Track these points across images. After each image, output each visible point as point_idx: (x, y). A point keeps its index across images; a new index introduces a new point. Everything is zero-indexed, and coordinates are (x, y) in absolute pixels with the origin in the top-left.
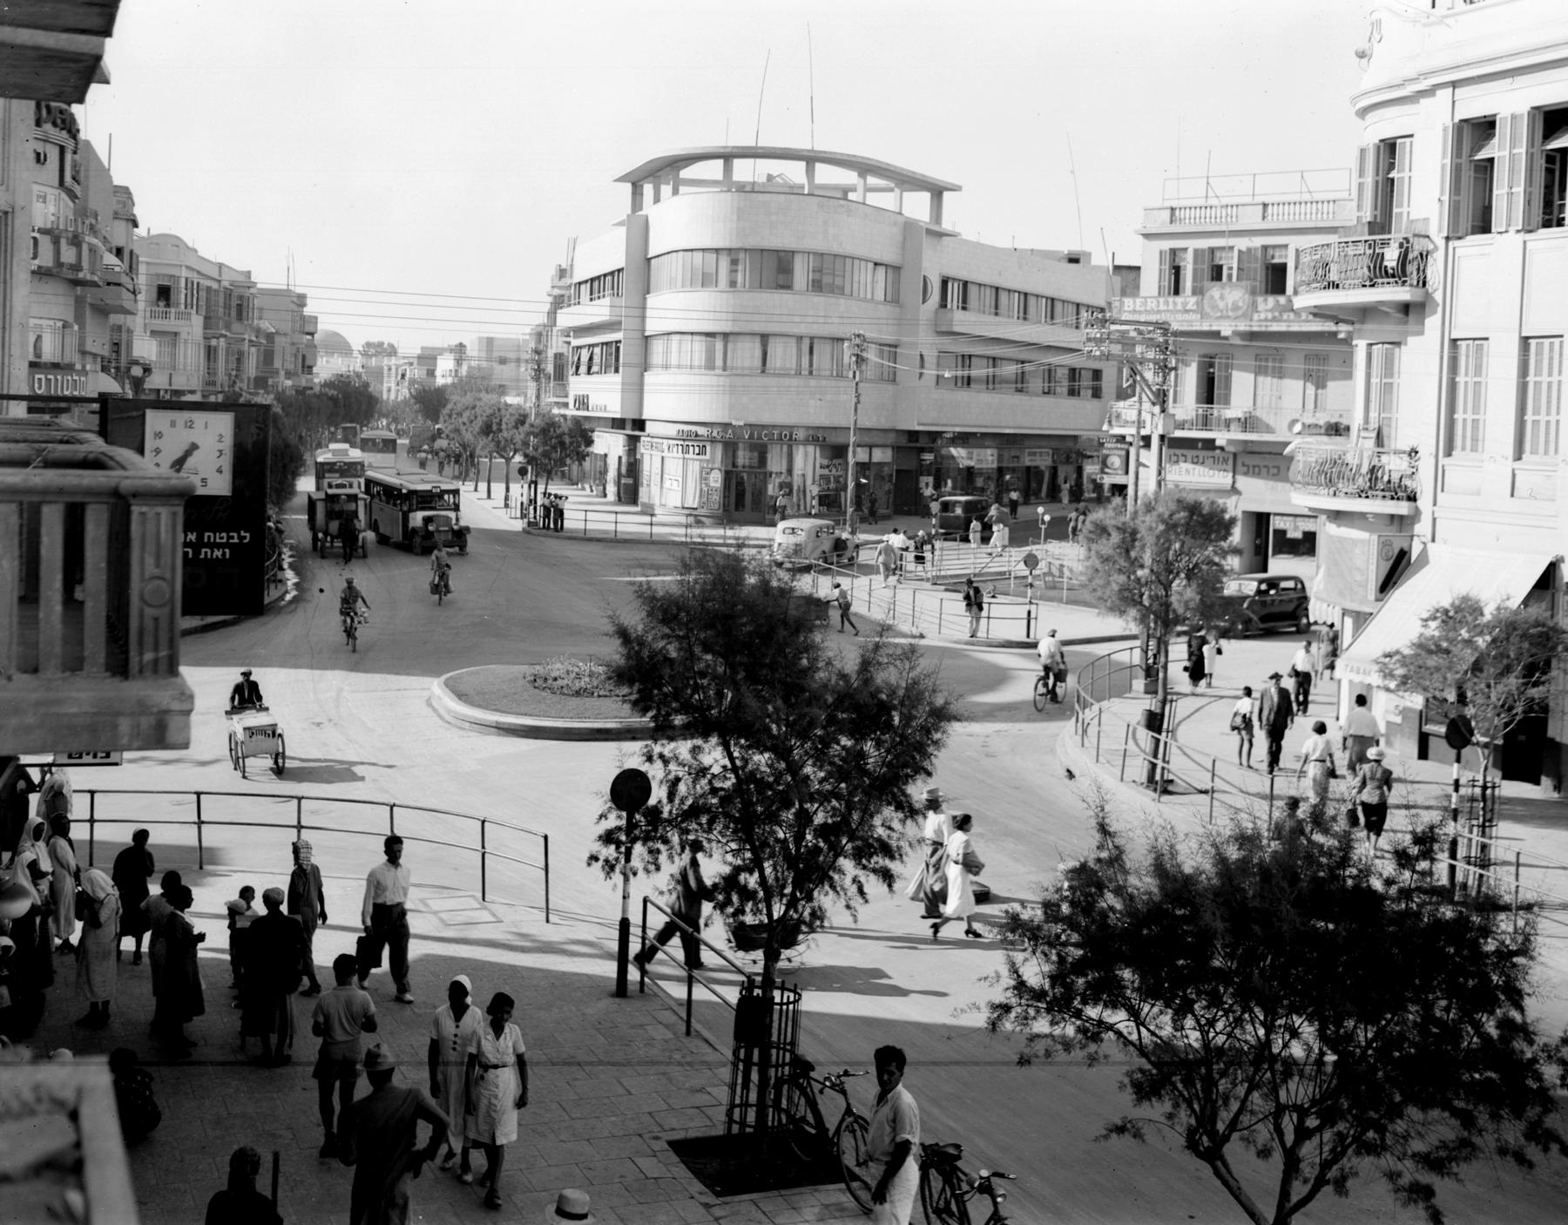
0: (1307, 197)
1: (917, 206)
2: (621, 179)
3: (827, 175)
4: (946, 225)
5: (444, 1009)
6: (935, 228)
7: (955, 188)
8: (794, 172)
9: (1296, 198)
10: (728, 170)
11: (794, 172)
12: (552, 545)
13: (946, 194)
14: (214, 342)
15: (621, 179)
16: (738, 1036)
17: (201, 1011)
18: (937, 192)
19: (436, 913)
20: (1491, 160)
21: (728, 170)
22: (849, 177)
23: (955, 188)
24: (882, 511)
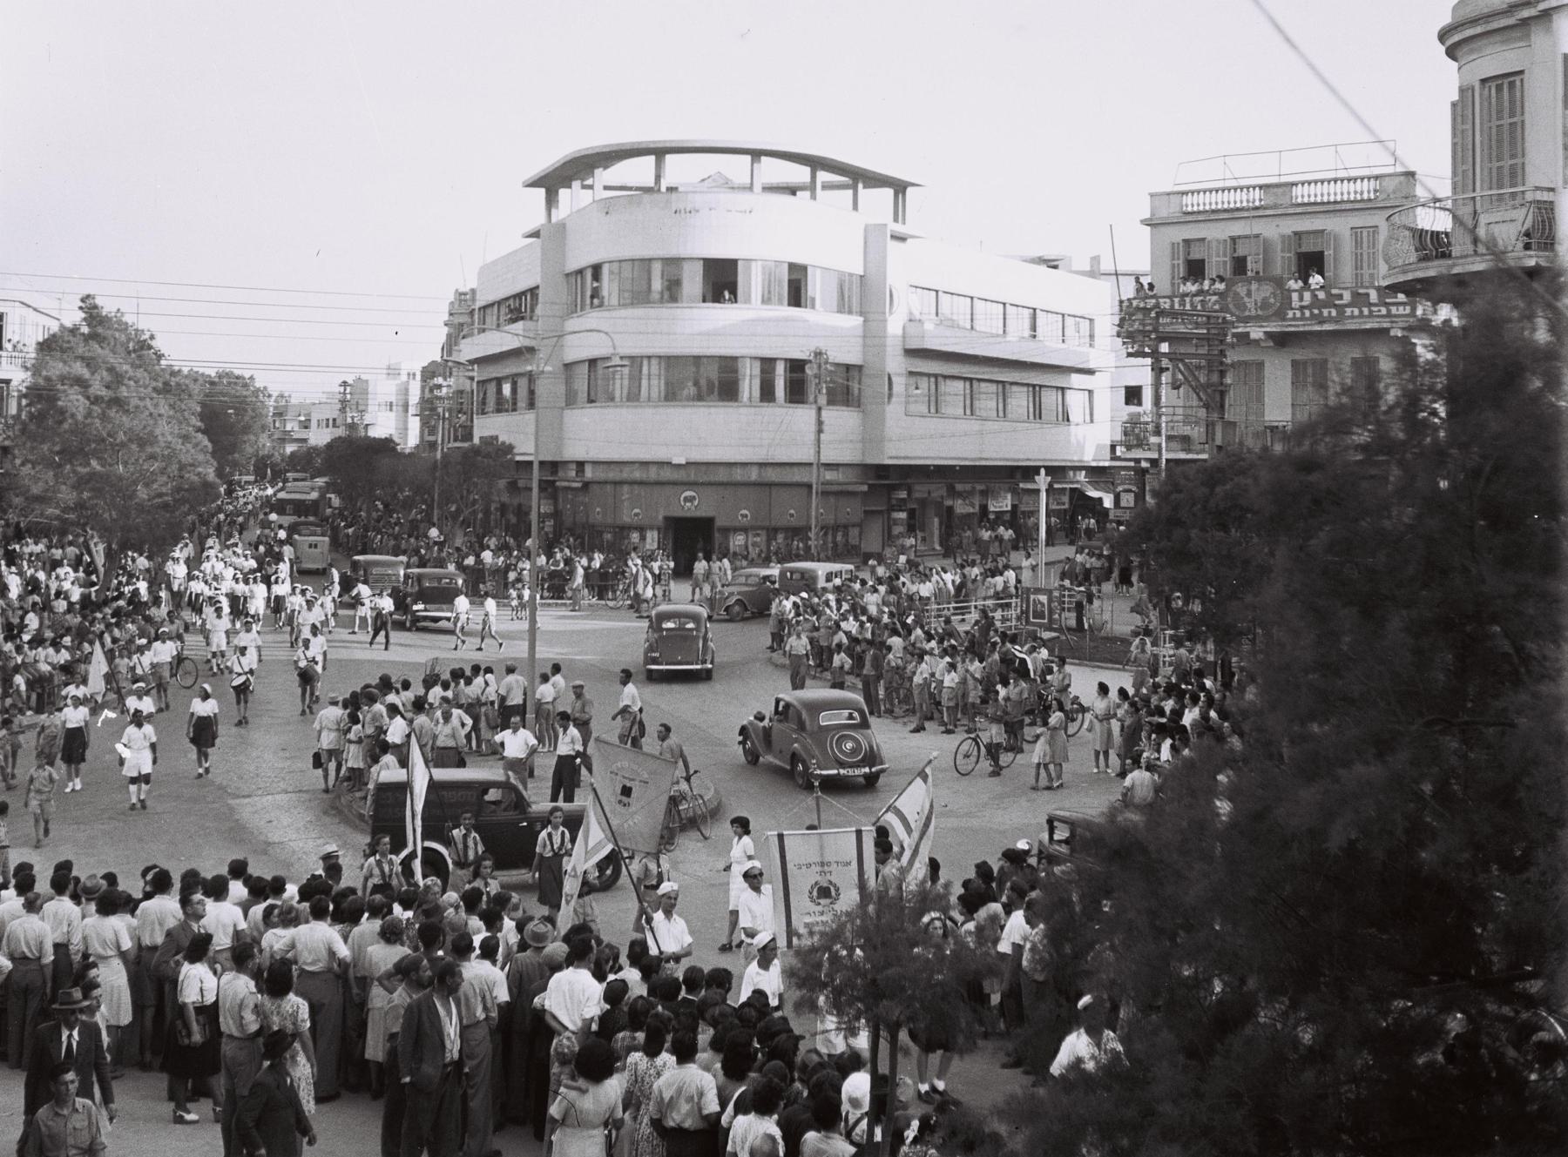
2: (534, 184)
15: (534, 184)
22: (801, 174)
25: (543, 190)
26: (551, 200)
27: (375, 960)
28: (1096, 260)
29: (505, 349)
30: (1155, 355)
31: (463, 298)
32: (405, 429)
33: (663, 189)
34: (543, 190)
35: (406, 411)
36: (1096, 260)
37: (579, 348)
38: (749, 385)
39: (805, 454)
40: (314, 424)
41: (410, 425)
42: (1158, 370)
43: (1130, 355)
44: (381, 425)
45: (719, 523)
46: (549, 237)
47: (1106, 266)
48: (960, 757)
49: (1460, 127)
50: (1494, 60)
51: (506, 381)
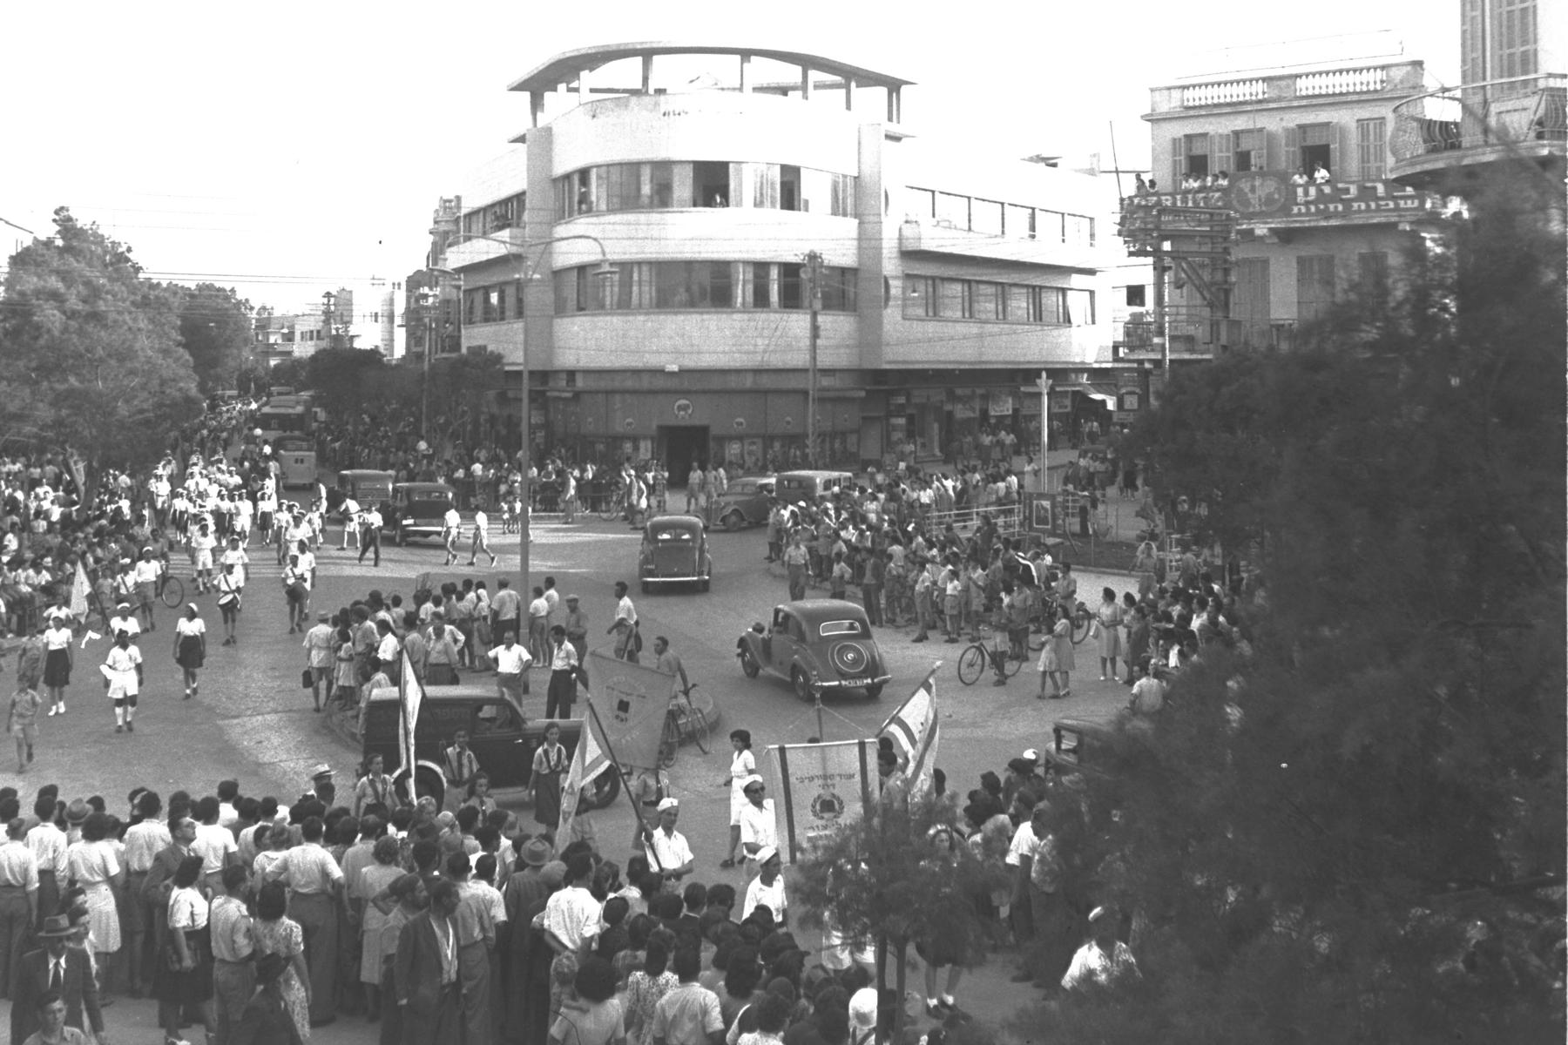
2: (520, 87)
15: (520, 87)
30: (1157, 254)
42: (1160, 270)
43: (1131, 254)
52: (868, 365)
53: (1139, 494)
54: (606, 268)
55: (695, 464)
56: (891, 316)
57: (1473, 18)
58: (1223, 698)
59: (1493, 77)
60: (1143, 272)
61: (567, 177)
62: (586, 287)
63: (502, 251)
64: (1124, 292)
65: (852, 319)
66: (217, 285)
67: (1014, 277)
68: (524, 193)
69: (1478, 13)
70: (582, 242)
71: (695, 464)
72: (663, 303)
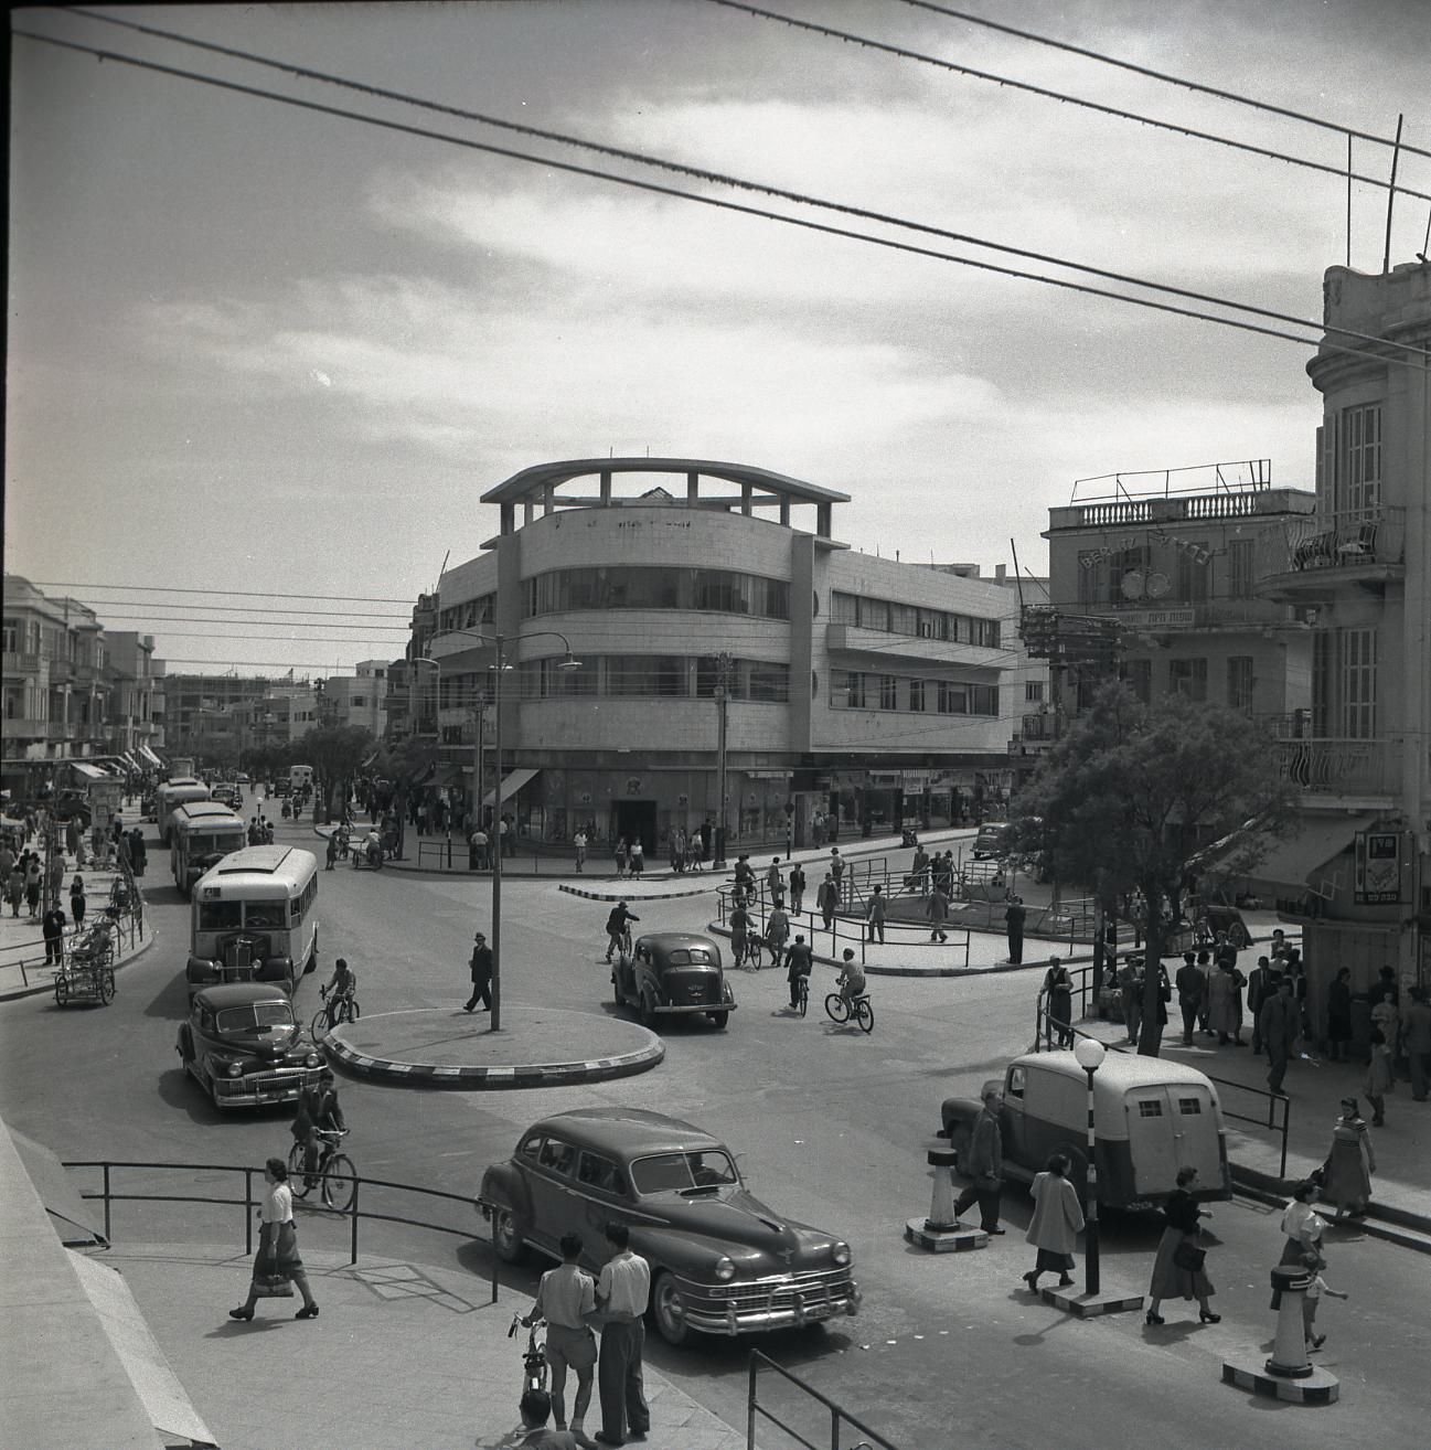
0: (1223, 491)
1: (804, 518)
2: (486, 499)
3: (710, 487)
4: (837, 536)
5: (1212, 1039)
6: (823, 540)
7: (845, 499)
8: (676, 485)
9: (1213, 492)
10: (606, 485)
11: (676, 485)
12: (746, 518)
13: (835, 506)
14: (60, 689)
15: (486, 499)
16: (1105, 1305)
17: (1311, 368)
18: (825, 502)
19: (369, 1285)
20: (291, 1295)
21: (606, 485)
22: (733, 490)
23: (845, 499)
24: (807, 840)
25: (499, 506)
26: (507, 517)
27: (621, 1309)
28: (1001, 568)
29: (669, 474)
30: (1054, 656)
31: (426, 605)
32: (374, 725)
33: (609, 504)
34: (499, 506)
35: (376, 706)
36: (1001, 568)
37: (533, 649)
38: (692, 674)
39: (1002, 636)
40: (292, 716)
41: (379, 718)
42: (1056, 670)
43: (1031, 655)
44: (357, 718)
45: (661, 807)
46: (506, 545)
47: (1010, 573)
48: (316, 1028)
49: (1325, 451)
50: (1358, 394)
51: (465, 680)
52: (799, 749)
53: (1086, 730)
54: (100, 634)
55: (638, 841)
56: (818, 705)
57: (1328, 455)
58: (1102, 966)
59: (1342, 509)
60: (1041, 672)
61: (527, 581)
62: (580, 679)
63: (478, 643)
64: (1023, 689)
65: (782, 708)
66: (247, 673)
67: (901, 672)
68: (495, 593)
69: (1333, 452)
70: (549, 636)
71: (638, 841)
72: (620, 690)
